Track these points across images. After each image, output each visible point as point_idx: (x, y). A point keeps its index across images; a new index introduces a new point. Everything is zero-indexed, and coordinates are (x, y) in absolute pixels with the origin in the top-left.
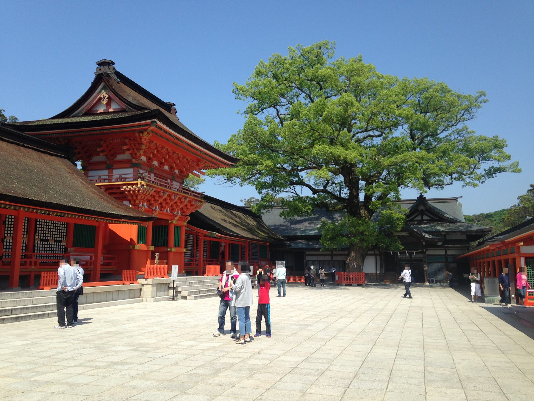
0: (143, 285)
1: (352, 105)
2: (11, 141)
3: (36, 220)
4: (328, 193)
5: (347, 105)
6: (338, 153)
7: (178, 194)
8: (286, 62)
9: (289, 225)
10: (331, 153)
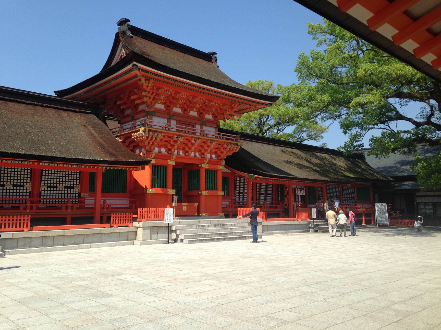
0: (137, 227)
3: (42, 170)
9: (399, 166)
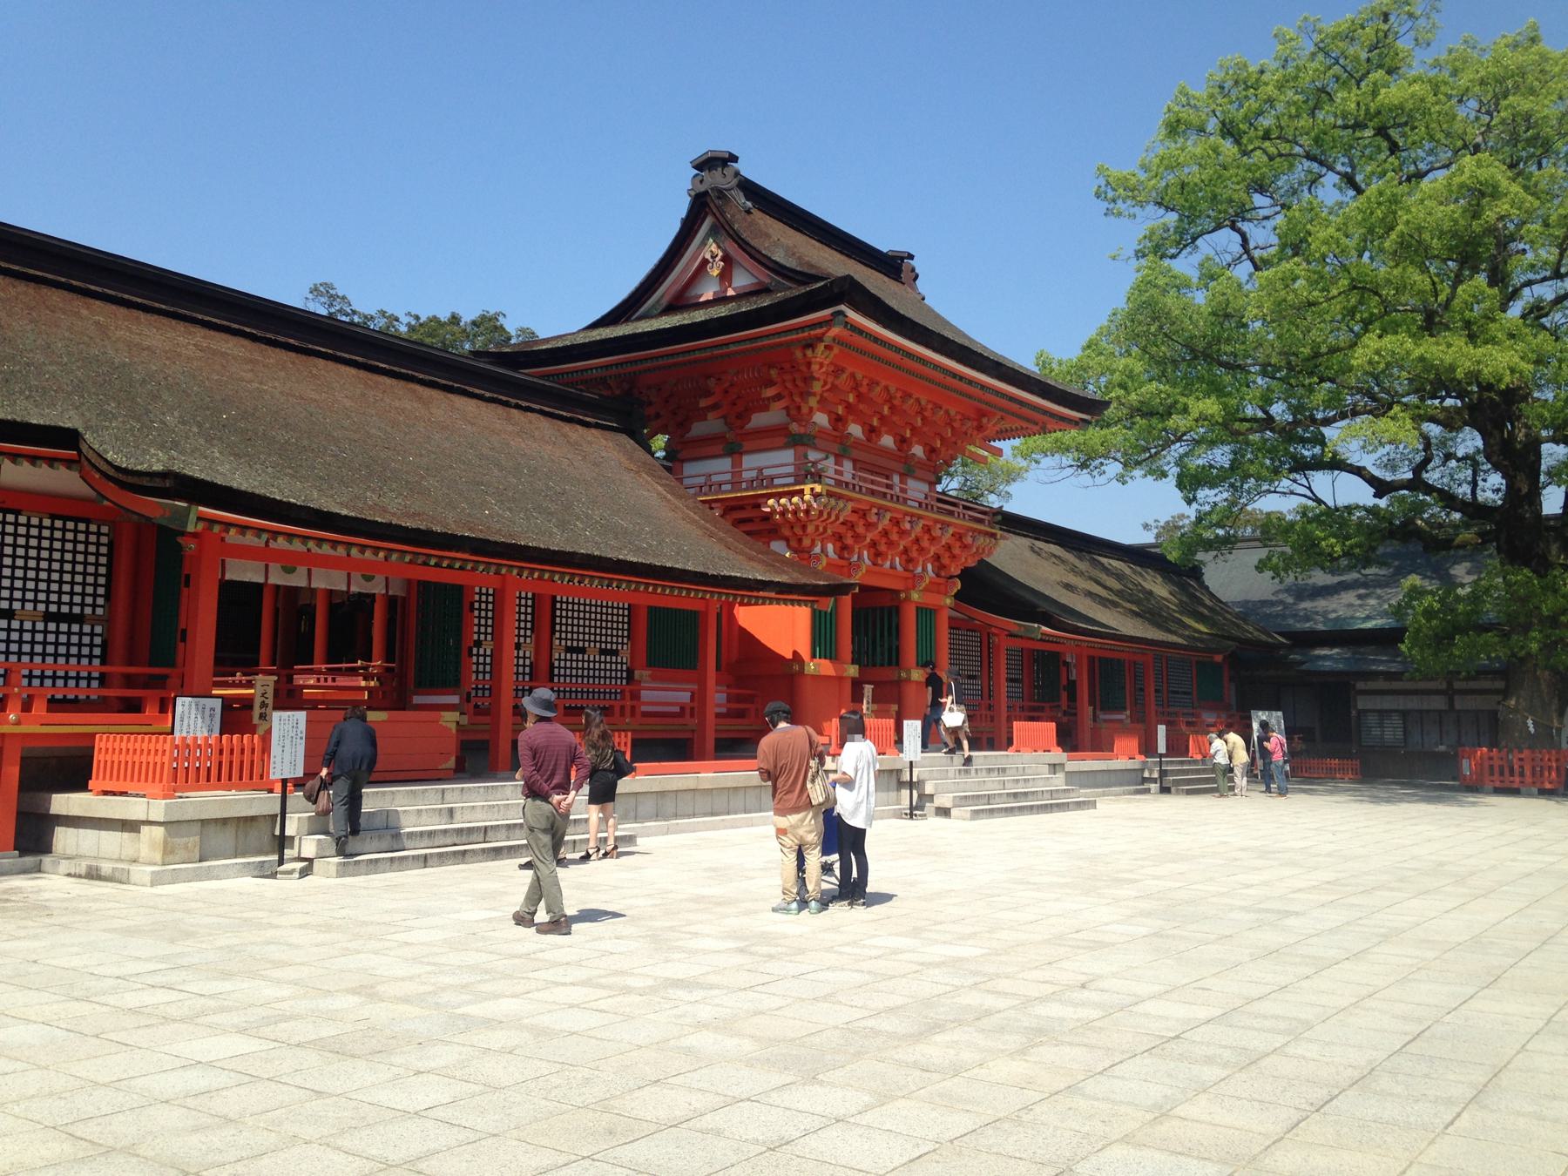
1: (1495, 193)
2: (488, 395)
4: (1429, 489)
5: (1481, 193)
6: (1448, 359)
7: (920, 517)
8: (1265, 78)
9: (1290, 600)
10: (1422, 359)
